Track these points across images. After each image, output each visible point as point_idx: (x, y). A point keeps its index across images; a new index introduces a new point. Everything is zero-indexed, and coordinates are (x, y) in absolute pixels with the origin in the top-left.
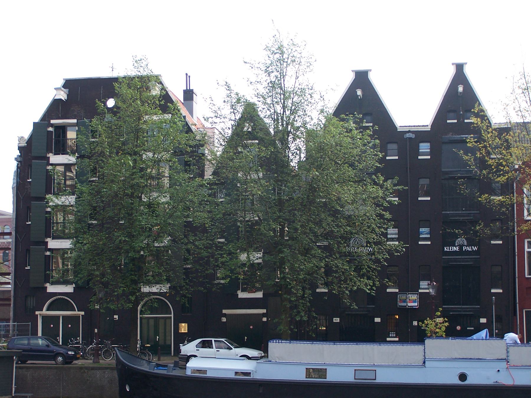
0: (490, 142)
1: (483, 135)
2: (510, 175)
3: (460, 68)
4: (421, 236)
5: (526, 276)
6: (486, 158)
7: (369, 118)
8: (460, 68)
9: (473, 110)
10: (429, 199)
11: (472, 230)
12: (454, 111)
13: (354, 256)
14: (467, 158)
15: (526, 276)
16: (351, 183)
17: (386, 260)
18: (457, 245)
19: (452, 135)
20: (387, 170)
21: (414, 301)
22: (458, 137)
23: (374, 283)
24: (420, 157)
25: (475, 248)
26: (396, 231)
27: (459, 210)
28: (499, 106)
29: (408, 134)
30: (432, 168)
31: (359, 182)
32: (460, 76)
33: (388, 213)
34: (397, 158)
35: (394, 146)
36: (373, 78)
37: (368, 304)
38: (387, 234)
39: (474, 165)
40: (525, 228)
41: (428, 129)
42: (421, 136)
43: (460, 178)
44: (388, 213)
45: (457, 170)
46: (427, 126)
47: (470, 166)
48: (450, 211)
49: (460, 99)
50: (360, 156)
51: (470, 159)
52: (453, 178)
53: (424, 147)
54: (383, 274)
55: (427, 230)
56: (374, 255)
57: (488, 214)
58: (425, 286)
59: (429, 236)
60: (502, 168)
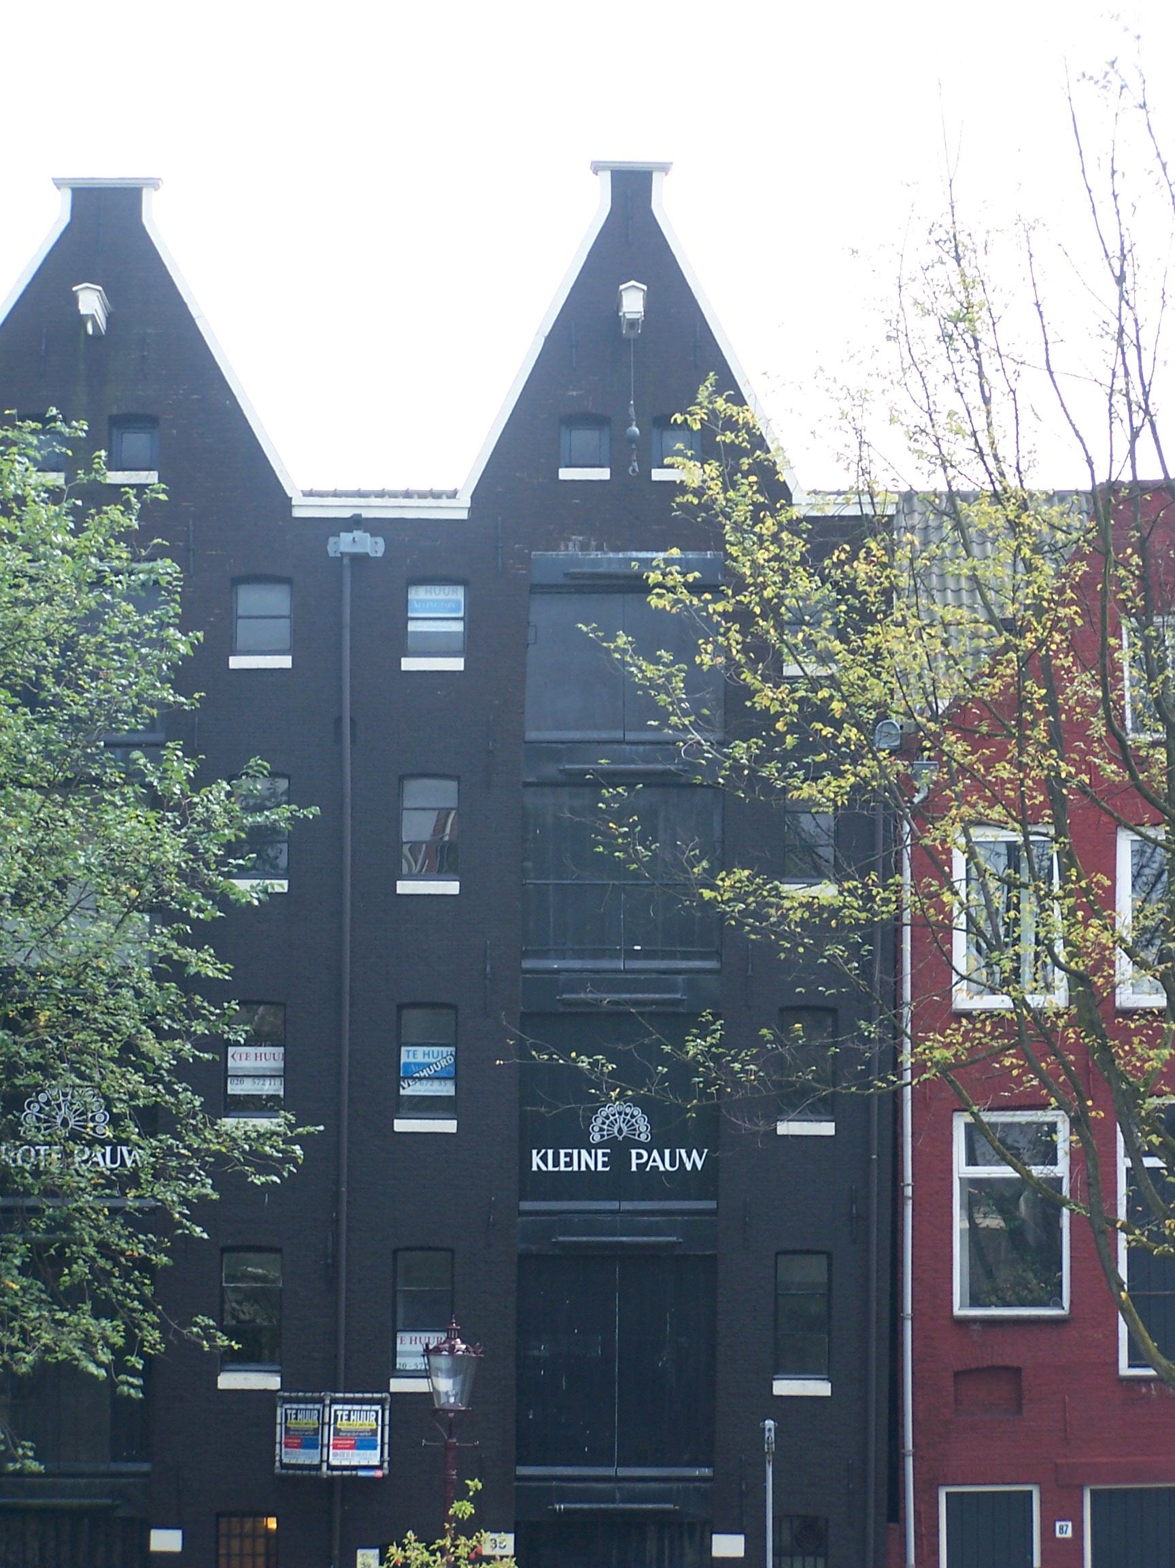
0: (768, 593)
1: (734, 551)
2: (863, 771)
3: (632, 188)
4: (410, 1089)
5: (958, 1311)
6: (747, 676)
7: (136, 442)
8: (632, 188)
9: (679, 418)
10: (453, 888)
11: (664, 1059)
12: (597, 421)
13: (27, 1193)
14: (651, 670)
15: (958, 1311)
16: (28, 795)
17: (199, 1210)
18: (596, 1138)
19: (584, 547)
20: (217, 722)
21: (363, 1442)
22: (607, 559)
23: (129, 1335)
24: (408, 664)
25: (695, 1160)
26: (270, 1058)
27: (614, 955)
28: (827, 400)
29: (346, 537)
30: (473, 726)
31: (67, 786)
32: (631, 236)
33: (208, 953)
34: (285, 662)
35: (276, 600)
36: (166, 225)
37: (115, 1458)
38: (220, 1072)
39: (685, 713)
40: (937, 1054)
41: (459, 510)
42: (418, 550)
43: (612, 779)
44: (208, 953)
45: (604, 735)
46: (453, 495)
47: (663, 715)
48: (561, 955)
49: (629, 355)
50: (69, 644)
51: (669, 677)
52: (575, 781)
53: (436, 610)
54: (184, 1283)
55: (439, 1056)
56: (138, 1185)
57: (752, 977)
58: (426, 1367)
59: (446, 1089)
60: (827, 731)
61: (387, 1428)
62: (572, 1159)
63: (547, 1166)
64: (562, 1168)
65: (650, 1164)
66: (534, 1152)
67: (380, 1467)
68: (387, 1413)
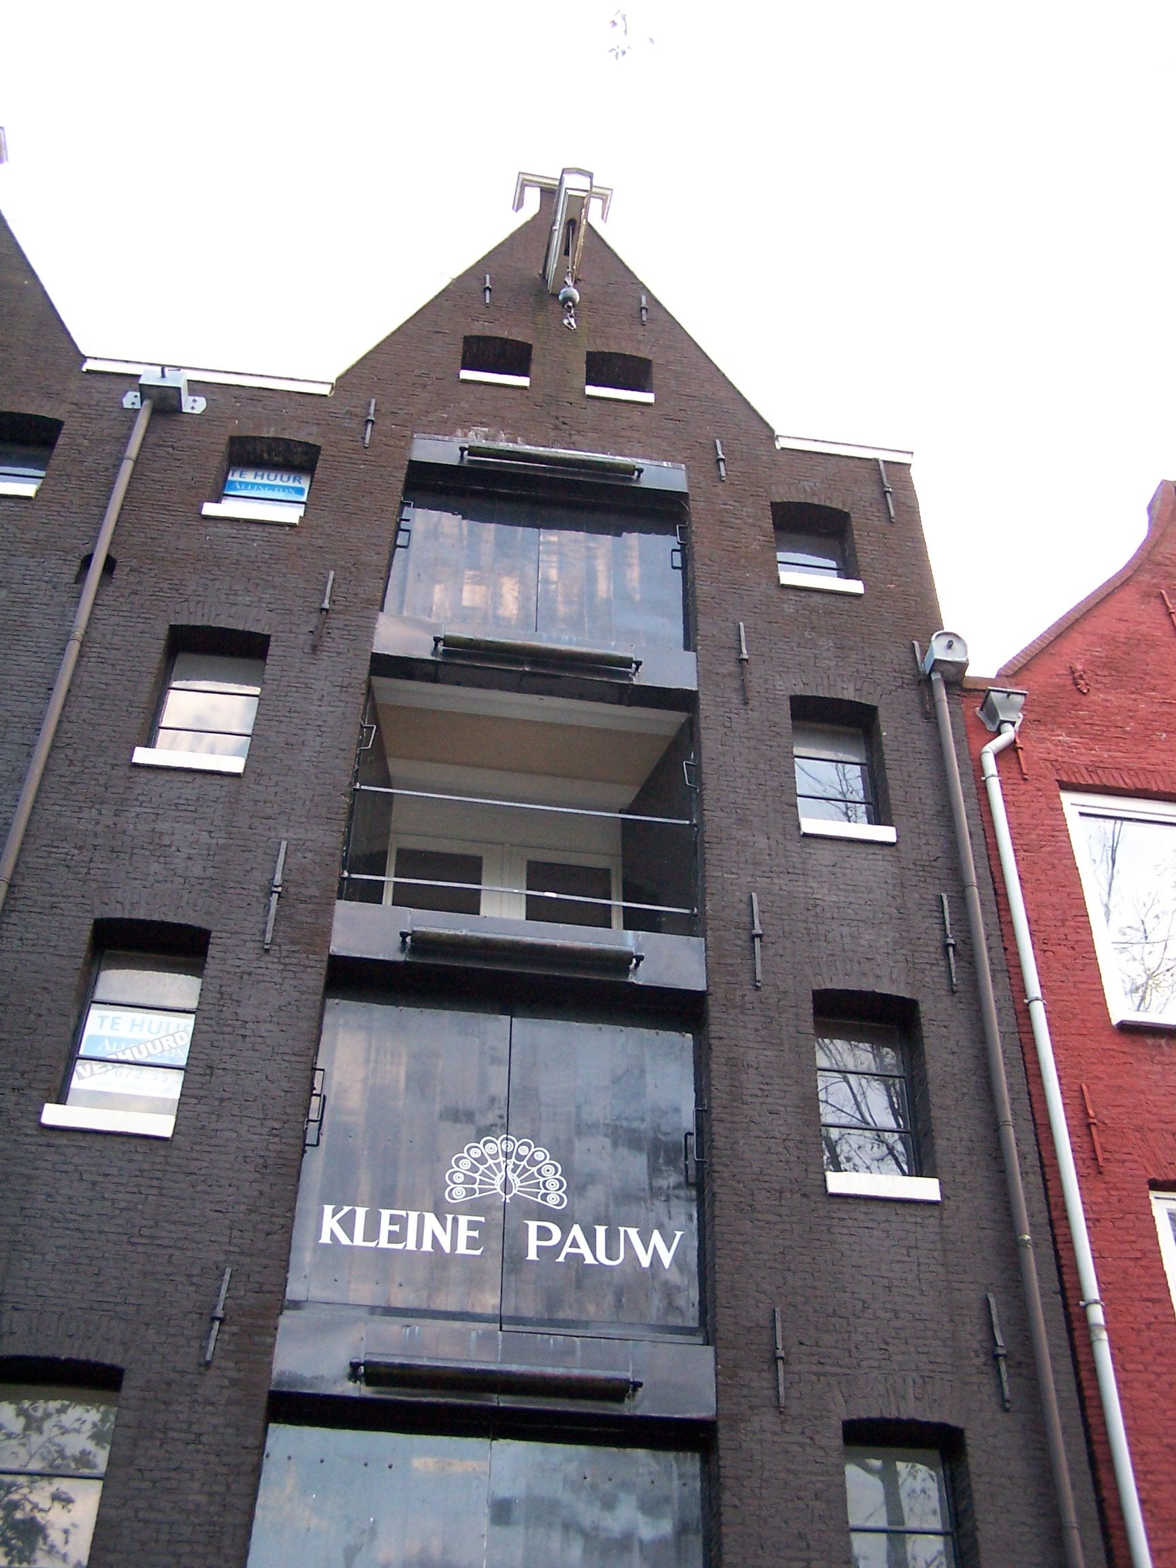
62: (404, 1228)
63: (351, 1236)
64: (383, 1243)
65: (567, 1249)
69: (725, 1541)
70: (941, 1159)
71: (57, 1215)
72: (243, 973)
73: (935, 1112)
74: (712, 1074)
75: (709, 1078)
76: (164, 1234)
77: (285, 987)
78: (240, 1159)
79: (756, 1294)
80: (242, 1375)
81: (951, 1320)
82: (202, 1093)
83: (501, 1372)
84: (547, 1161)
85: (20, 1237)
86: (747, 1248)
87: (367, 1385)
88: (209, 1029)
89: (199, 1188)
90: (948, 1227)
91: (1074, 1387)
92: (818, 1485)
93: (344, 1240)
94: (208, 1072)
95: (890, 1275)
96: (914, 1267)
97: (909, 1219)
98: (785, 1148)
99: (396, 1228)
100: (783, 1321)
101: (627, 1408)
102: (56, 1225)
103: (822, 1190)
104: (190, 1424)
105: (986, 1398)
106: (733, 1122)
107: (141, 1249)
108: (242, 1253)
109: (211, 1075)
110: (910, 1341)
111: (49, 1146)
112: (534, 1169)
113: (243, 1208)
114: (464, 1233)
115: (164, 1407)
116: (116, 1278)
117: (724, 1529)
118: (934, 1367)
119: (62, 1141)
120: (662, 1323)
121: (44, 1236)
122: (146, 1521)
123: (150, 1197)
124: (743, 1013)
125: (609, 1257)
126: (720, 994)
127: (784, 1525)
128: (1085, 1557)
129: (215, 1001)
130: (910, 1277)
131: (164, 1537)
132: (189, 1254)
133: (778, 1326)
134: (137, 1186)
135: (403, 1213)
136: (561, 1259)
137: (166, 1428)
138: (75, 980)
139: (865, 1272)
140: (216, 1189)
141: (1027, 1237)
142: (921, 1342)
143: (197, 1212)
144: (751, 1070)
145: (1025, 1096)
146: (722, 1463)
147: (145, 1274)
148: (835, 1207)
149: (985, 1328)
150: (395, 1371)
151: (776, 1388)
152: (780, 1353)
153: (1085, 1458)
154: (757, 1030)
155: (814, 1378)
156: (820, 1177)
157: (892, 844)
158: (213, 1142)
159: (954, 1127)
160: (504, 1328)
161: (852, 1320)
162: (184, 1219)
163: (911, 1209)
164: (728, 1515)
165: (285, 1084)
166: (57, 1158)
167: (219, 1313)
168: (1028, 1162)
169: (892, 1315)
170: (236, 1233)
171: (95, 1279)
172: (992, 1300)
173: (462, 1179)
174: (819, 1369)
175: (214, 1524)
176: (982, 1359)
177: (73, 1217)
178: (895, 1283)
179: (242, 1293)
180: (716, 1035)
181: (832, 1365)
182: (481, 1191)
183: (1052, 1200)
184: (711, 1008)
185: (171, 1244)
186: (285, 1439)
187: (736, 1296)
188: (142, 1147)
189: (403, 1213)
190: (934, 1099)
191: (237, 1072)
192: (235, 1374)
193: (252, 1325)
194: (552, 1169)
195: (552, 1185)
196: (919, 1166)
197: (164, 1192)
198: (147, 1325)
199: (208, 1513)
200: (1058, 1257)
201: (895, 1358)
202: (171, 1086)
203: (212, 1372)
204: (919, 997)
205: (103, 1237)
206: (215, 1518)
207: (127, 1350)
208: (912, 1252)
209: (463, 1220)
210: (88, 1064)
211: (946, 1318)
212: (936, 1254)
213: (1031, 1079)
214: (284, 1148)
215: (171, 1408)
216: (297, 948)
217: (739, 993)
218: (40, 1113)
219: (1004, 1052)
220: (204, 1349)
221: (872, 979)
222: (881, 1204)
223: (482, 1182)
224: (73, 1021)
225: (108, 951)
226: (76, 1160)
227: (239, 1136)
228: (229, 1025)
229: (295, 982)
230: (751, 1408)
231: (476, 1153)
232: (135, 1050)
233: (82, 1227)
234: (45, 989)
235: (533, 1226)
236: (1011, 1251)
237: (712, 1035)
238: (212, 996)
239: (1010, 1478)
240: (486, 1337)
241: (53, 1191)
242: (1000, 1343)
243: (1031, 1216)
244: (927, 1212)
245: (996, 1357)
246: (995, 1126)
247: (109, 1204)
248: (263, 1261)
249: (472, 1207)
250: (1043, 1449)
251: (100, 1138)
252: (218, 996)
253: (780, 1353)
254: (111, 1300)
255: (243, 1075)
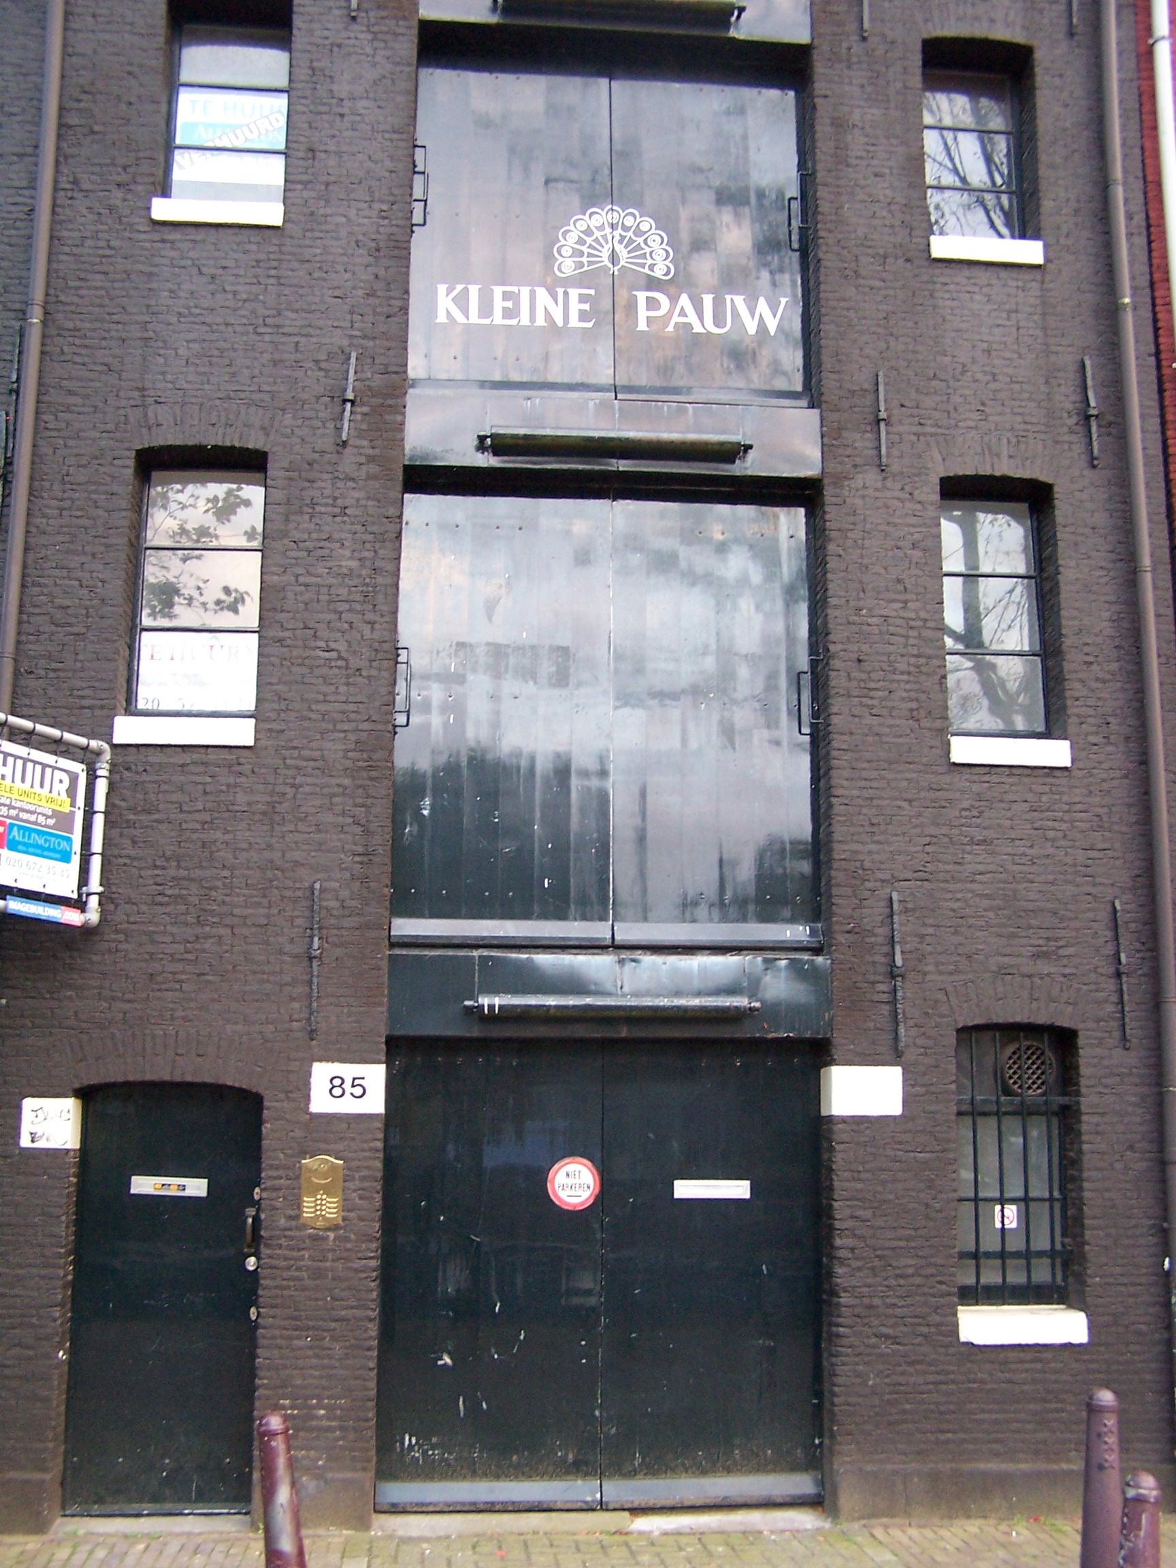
18: (567, 266)
61: (99, 821)
62: (517, 304)
63: (466, 314)
64: (498, 319)
65: (676, 319)
66: (442, 289)
67: (79, 904)
68: (102, 787)
69: (830, 586)
70: (1046, 221)
71: (182, 310)
72: (332, 45)
73: (1043, 171)
74: (817, 135)
75: (813, 141)
76: (288, 322)
77: (377, 59)
78: (353, 244)
79: (861, 360)
80: (377, 451)
81: (1047, 382)
82: (305, 178)
83: (619, 439)
84: (653, 231)
85: (151, 334)
86: (852, 314)
87: (495, 455)
88: (305, 109)
89: (316, 275)
90: (1051, 290)
91: (1159, 445)
92: (916, 536)
93: (460, 318)
94: (310, 155)
95: (991, 339)
96: (1014, 330)
97: (1011, 283)
98: (890, 211)
99: (509, 304)
100: (886, 384)
101: (739, 469)
102: (182, 319)
103: (926, 255)
104: (335, 499)
105: (1076, 457)
106: (838, 186)
107: (267, 338)
108: (365, 337)
109: (314, 158)
110: (1006, 403)
111: (163, 241)
112: (640, 240)
113: (360, 292)
114: (575, 307)
115: (308, 484)
116: (248, 367)
117: (829, 576)
118: (1029, 427)
119: (175, 236)
120: (768, 387)
121: (174, 332)
122: (307, 585)
123: (269, 287)
124: (849, 67)
125: (717, 324)
126: (825, 48)
127: (883, 571)
128: (1155, 595)
129: (308, 78)
130: (1010, 340)
131: (324, 598)
132: (314, 340)
133: (881, 388)
134: (256, 277)
135: (514, 289)
136: (670, 328)
137: (313, 504)
138: (158, 62)
139: (965, 336)
140: (333, 275)
141: (1127, 300)
142: (1017, 403)
143: (317, 300)
144: (857, 131)
145: (1137, 151)
146: (827, 517)
147: (275, 363)
148: (938, 271)
149: (1078, 390)
150: (521, 442)
151: (879, 448)
152: (883, 415)
153: (1163, 509)
154: (862, 86)
155: (914, 438)
156: (924, 241)
157: (1039, 266)
158: (323, 227)
159: (1061, 189)
160: (619, 396)
161: (951, 383)
162: (305, 307)
163: (1014, 273)
164: (832, 563)
165: (389, 164)
166: (173, 254)
167: (350, 396)
168: (1134, 222)
169: (989, 378)
170: (357, 317)
171: (228, 369)
172: (1088, 363)
173: (571, 251)
174: (919, 429)
175: (367, 585)
176: (1074, 419)
177: (198, 311)
178: (995, 346)
179: (369, 375)
180: (823, 92)
181: (932, 426)
182: (590, 263)
183: (1155, 261)
184: (816, 64)
185: (296, 331)
186: (421, 509)
187: (840, 361)
188: (255, 237)
189: (514, 289)
190: (1043, 158)
191: (339, 154)
192: (370, 452)
193: (382, 405)
194: (658, 239)
195: (659, 255)
196: (1024, 227)
197: (282, 281)
198: (283, 410)
199: (359, 576)
200: (1155, 321)
201: (990, 418)
202: (274, 171)
203: (348, 450)
204: (1035, 43)
205: (230, 329)
206: (368, 580)
207: (267, 435)
208: (1013, 315)
209: (574, 293)
210: (186, 153)
211: (1042, 380)
212: (1036, 317)
213: (1146, 132)
214: (395, 230)
215: (315, 485)
216: (384, 13)
217: (845, 45)
218: (149, 209)
219: (1121, 102)
220: (339, 429)
221: (985, 24)
222: (984, 268)
223: (589, 255)
224: (164, 108)
225: (186, 26)
226: (191, 254)
227: (349, 220)
228: (325, 104)
229: (388, 53)
230: (855, 466)
231: (582, 226)
232: (231, 135)
233: (208, 320)
234: (130, 73)
235: (642, 296)
236: (1110, 314)
237: (817, 92)
238: (303, 73)
239: (1093, 528)
240: (603, 405)
241: (175, 287)
242: (1093, 404)
243: (1133, 278)
244: (1027, 276)
245: (1088, 418)
246: (1104, 186)
247: (230, 296)
248: (387, 344)
249: (581, 280)
250: (1125, 502)
251: (213, 231)
252: (310, 72)
253: (883, 415)
254: (245, 388)
255: (346, 157)
